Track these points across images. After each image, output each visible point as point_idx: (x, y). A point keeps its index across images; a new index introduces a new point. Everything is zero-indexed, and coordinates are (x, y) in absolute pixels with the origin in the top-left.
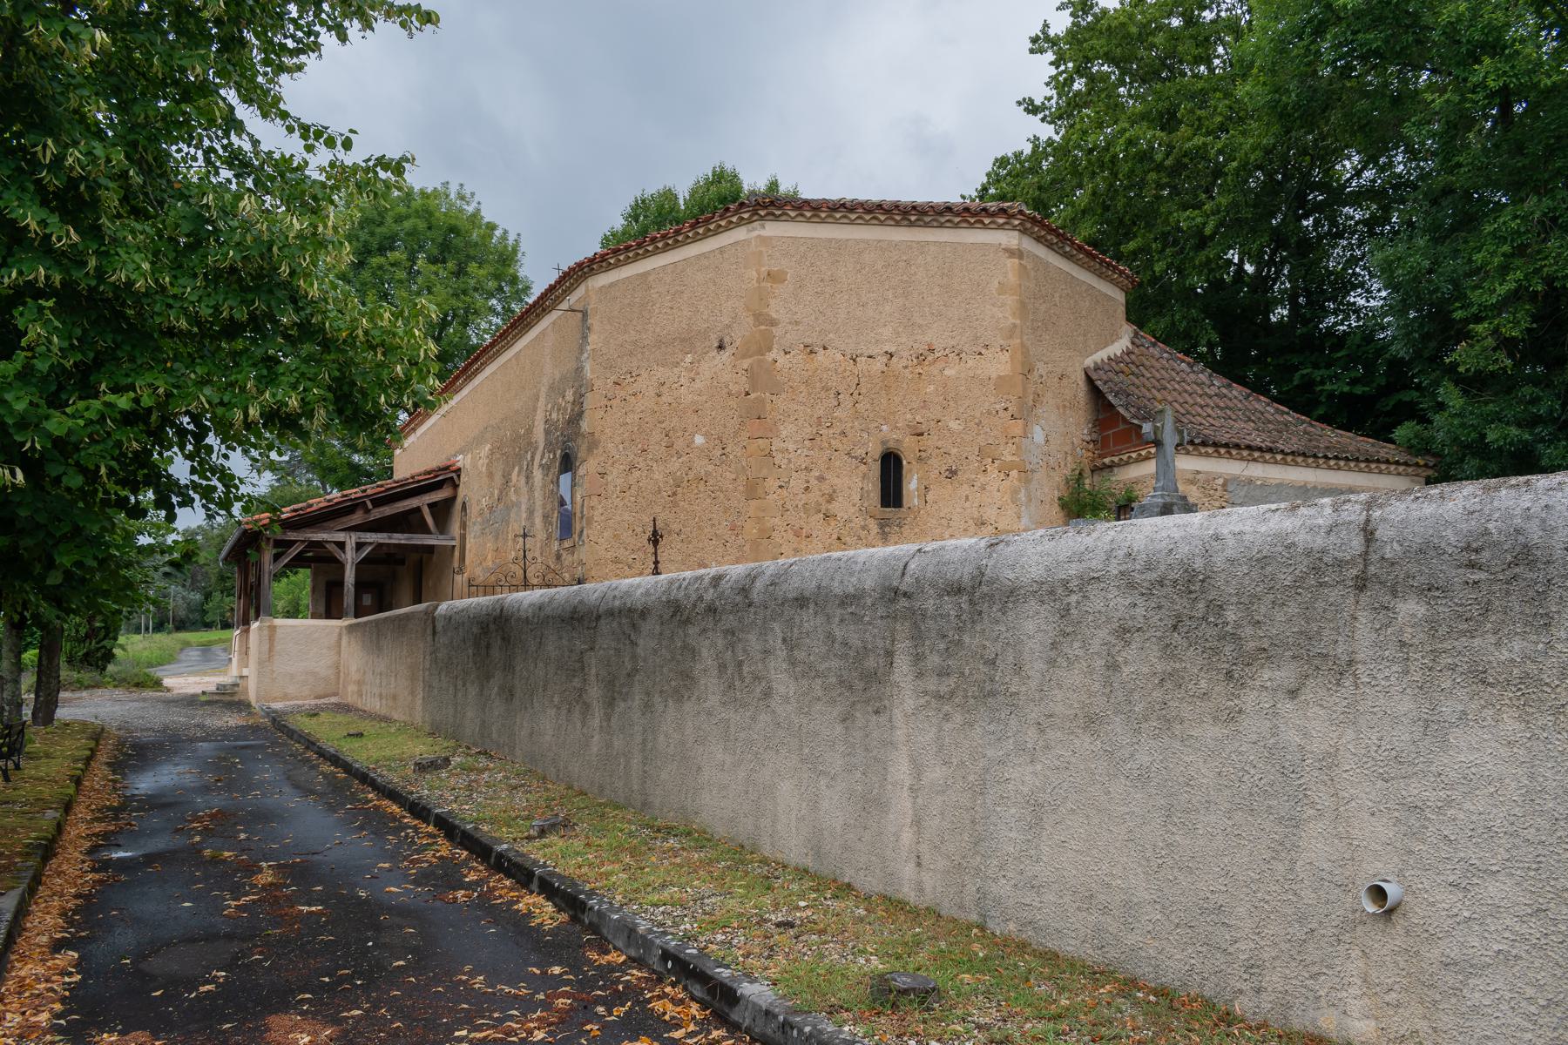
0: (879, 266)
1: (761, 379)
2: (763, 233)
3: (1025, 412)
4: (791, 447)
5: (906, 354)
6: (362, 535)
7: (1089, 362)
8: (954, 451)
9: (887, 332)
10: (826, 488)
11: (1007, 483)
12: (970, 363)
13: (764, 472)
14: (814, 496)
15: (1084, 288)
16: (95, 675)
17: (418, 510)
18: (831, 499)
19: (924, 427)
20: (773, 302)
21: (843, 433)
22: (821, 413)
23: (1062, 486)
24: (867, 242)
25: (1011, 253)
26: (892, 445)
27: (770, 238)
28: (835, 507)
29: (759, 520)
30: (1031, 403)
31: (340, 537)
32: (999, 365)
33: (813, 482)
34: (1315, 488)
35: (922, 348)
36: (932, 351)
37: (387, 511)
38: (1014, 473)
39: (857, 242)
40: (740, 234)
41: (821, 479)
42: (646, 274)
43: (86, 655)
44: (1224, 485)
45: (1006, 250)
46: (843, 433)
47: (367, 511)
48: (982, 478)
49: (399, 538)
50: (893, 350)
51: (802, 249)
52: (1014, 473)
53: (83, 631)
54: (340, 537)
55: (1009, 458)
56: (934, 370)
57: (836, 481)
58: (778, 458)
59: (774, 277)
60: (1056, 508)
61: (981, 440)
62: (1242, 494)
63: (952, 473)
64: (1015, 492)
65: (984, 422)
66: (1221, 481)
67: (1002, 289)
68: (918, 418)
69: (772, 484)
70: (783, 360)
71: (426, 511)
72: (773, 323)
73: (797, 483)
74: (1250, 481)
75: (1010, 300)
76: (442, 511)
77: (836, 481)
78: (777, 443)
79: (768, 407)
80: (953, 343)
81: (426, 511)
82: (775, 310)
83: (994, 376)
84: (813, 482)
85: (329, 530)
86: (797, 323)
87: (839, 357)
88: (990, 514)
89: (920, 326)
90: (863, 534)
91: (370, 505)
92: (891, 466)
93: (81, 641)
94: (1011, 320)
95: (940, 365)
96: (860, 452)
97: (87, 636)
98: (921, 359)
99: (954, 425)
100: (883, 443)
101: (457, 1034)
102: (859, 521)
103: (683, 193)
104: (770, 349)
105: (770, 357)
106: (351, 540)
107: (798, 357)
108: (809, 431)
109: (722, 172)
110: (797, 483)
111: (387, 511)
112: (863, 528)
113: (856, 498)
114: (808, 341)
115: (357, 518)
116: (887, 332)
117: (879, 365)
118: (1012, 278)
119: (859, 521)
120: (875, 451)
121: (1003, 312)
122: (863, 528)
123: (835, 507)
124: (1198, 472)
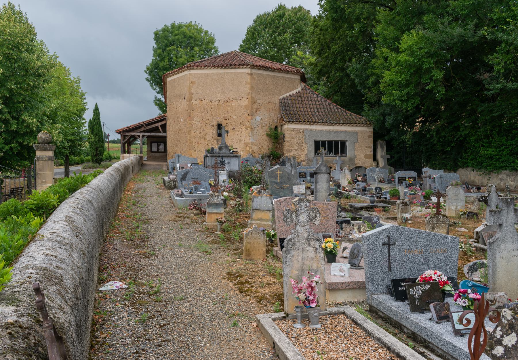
0: (217, 79)
1: (191, 107)
2: (190, 72)
3: (253, 114)
4: (197, 123)
5: (223, 100)
6: (143, 133)
7: (281, 97)
8: (234, 123)
9: (219, 95)
10: (205, 132)
11: (247, 131)
12: (238, 102)
13: (191, 129)
14: (202, 134)
15: (280, 78)
16: (98, 165)
17: (157, 127)
18: (206, 135)
19: (227, 118)
20: (192, 89)
21: (208, 120)
22: (203, 115)
23: (268, 130)
24: (214, 73)
25: (248, 74)
26: (219, 122)
27: (192, 74)
28: (206, 137)
29: (190, 140)
30: (255, 110)
31: (139, 134)
32: (246, 102)
33: (202, 131)
34: (333, 131)
35: (227, 99)
36: (229, 99)
37: (150, 127)
38: (249, 129)
39: (212, 73)
40: (186, 72)
41: (203, 130)
42: (174, 79)
43: (96, 160)
44: (303, 131)
45: (247, 73)
46: (208, 120)
47: (145, 127)
48: (241, 130)
49: (153, 134)
50: (220, 99)
51: (199, 76)
52: (249, 129)
53: (95, 154)
54: (139, 134)
55: (248, 125)
56: (230, 104)
57: (207, 131)
58: (194, 126)
59: (192, 83)
60: (265, 136)
61: (241, 121)
62: (309, 133)
63: (234, 129)
64: (249, 133)
65: (242, 116)
66: (302, 130)
67: (246, 83)
68: (226, 116)
69: (192, 131)
70: (195, 103)
71: (160, 127)
72: (192, 94)
73: (198, 132)
74: (312, 130)
75: (248, 86)
76: (164, 127)
77: (207, 131)
78: (194, 122)
79: (191, 114)
80: (234, 97)
81: (160, 127)
82: (193, 91)
83: (244, 105)
84: (202, 131)
85: (136, 132)
86: (198, 94)
87: (208, 101)
88: (243, 139)
89: (227, 93)
90: (213, 143)
91: (145, 126)
92: (220, 126)
93: (95, 156)
94: (249, 91)
95: (231, 103)
96: (212, 124)
97: (96, 155)
98: (227, 101)
99: (234, 117)
100: (218, 122)
101: (474, 337)
102: (212, 140)
103: (271, 12)
104: (192, 100)
105: (192, 102)
106: (141, 135)
107: (198, 102)
108: (201, 119)
109: (281, 5)
110: (198, 132)
111: (150, 127)
112: (213, 142)
113: (211, 135)
114: (200, 98)
115: (142, 129)
116: (219, 95)
117: (217, 103)
118: (249, 81)
119: (212, 140)
120: (215, 123)
121: (246, 89)
122: (213, 142)
123: (206, 137)
124: (295, 128)
